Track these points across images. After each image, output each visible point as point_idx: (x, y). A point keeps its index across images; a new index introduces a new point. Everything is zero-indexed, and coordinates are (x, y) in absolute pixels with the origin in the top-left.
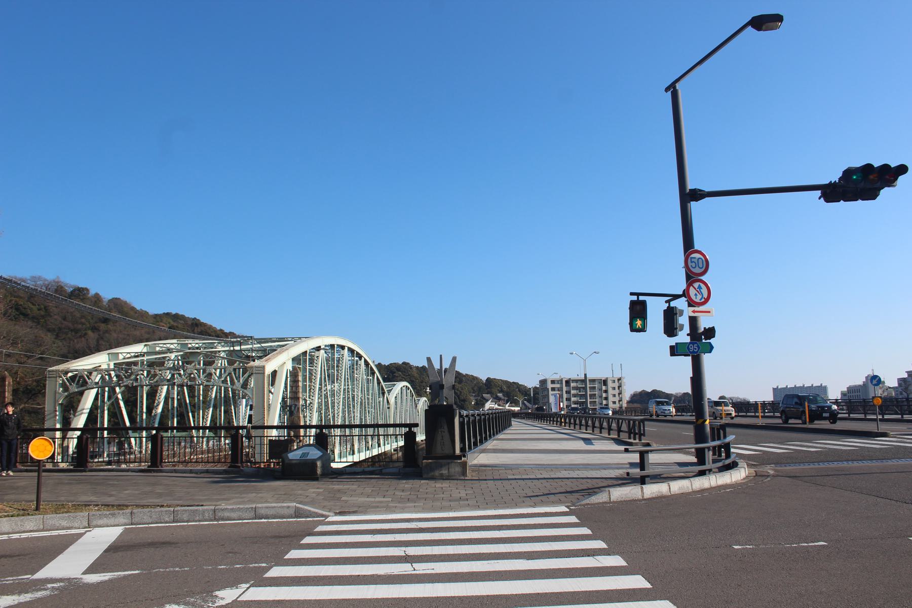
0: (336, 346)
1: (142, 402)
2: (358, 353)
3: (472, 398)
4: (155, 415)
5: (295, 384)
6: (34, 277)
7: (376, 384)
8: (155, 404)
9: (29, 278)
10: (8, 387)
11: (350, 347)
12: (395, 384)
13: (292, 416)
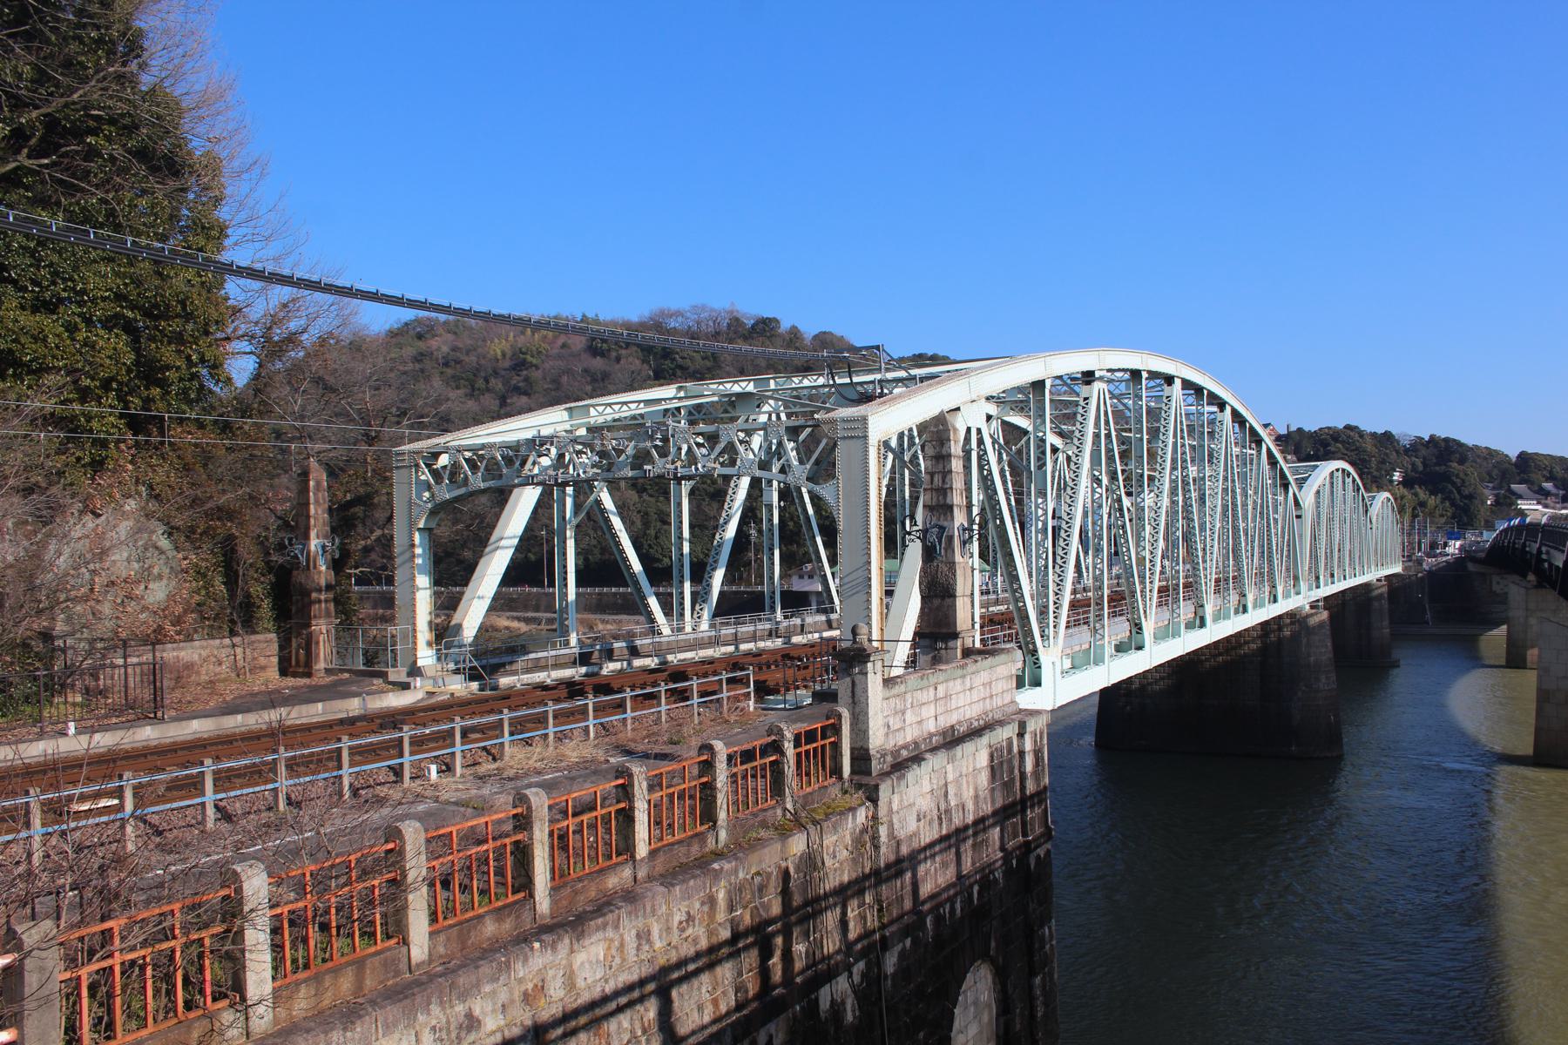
0: (1145, 375)
1: (680, 516)
2: (1211, 395)
3: (1486, 492)
4: (720, 545)
5: (940, 467)
6: (695, 307)
7: (1267, 467)
8: (722, 521)
9: (687, 308)
10: (314, 494)
11: (1213, 390)
12: (1317, 466)
13: (932, 561)
